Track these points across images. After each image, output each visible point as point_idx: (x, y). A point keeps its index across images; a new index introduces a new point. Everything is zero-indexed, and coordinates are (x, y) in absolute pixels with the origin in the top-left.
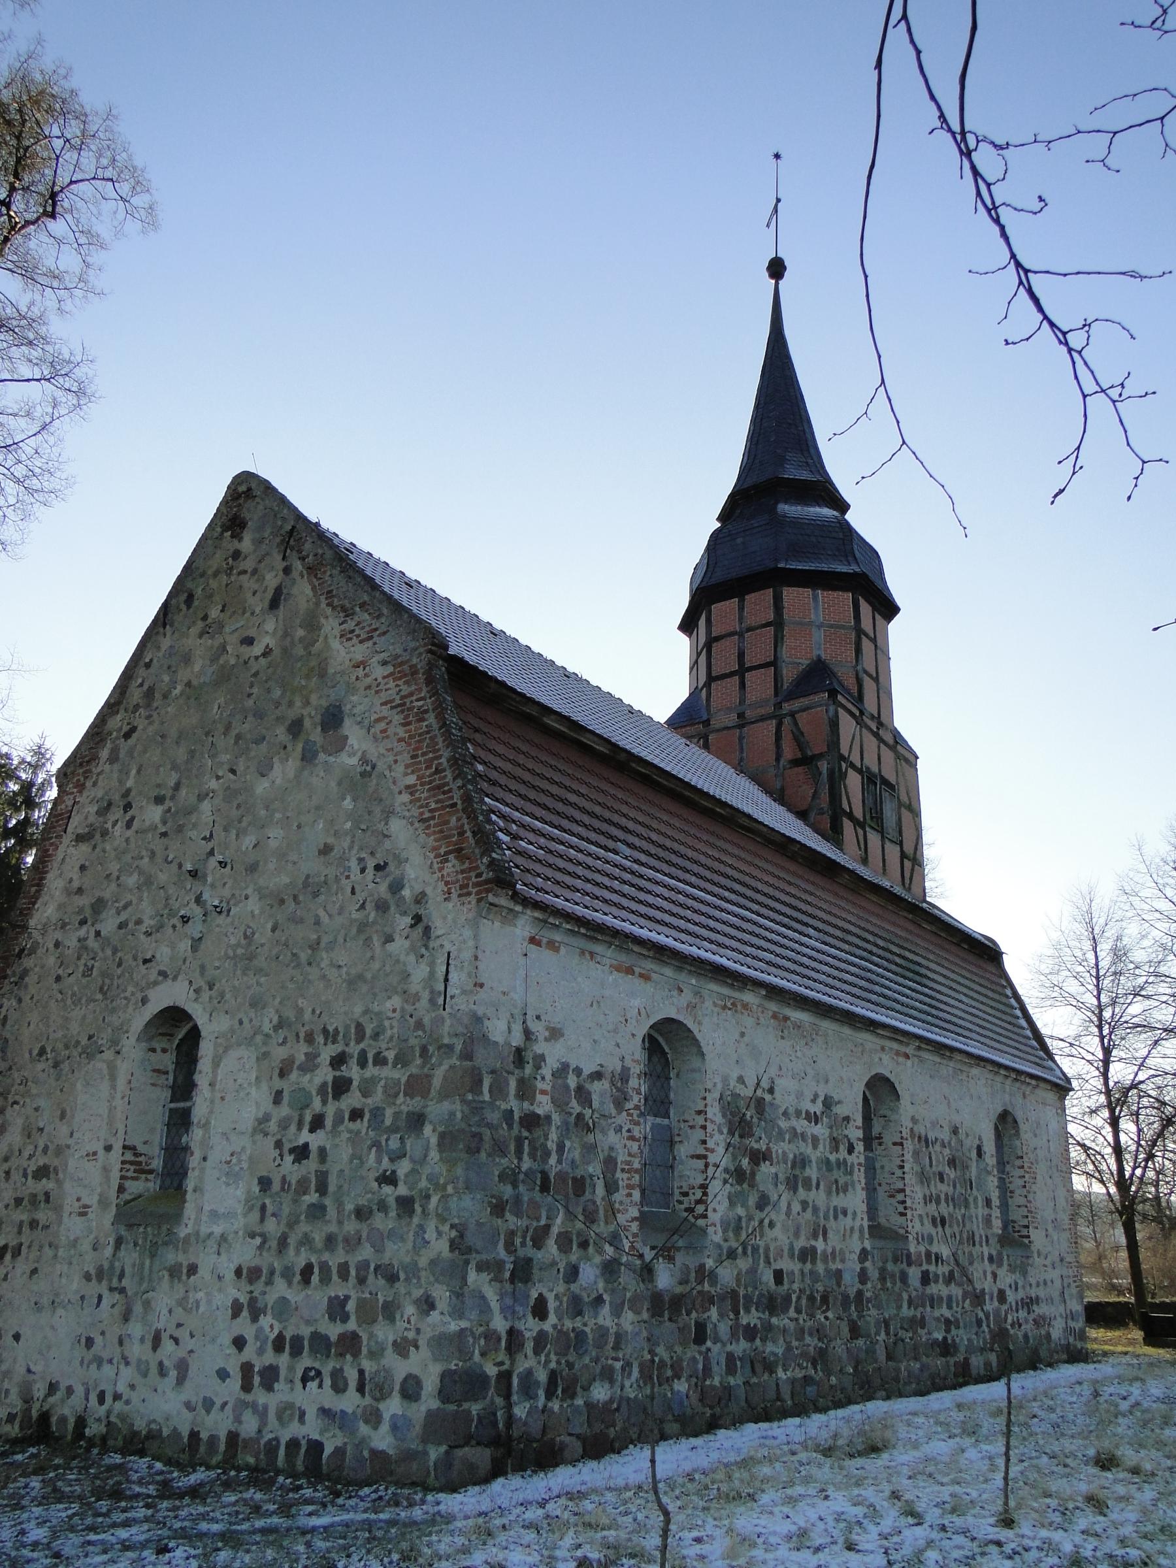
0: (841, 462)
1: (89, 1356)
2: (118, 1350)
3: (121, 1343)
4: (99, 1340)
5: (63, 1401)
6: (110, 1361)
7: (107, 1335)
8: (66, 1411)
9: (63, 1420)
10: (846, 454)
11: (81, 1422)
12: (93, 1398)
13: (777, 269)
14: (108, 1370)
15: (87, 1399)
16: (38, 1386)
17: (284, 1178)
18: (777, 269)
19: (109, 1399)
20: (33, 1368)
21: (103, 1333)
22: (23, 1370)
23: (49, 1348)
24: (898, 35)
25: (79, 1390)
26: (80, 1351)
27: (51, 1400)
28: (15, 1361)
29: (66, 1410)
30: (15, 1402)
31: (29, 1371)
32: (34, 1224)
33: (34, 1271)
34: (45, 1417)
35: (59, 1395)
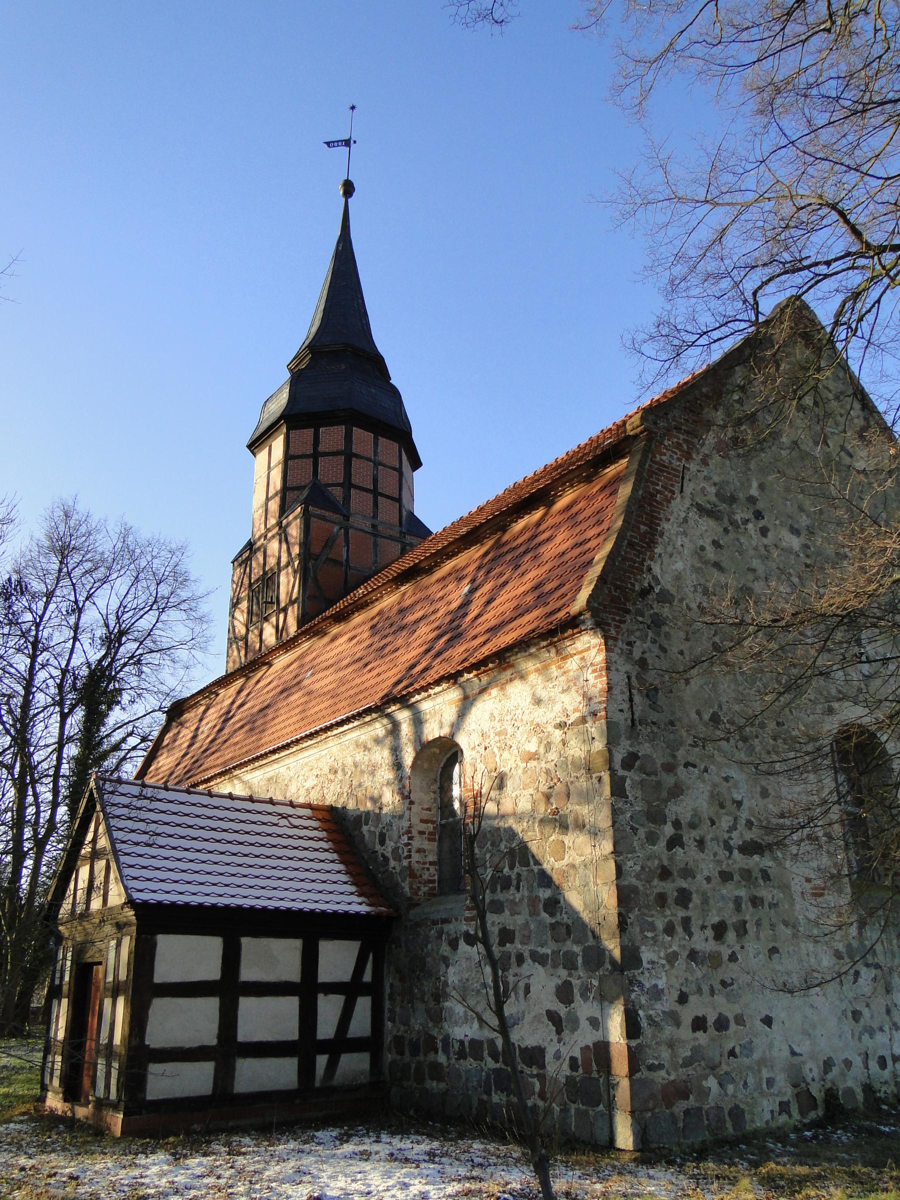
0: (385, 337)
1: (859, 1028)
2: (887, 1018)
3: (888, 1012)
4: (866, 1012)
5: (843, 1075)
6: (881, 1029)
7: (872, 1006)
8: (850, 1083)
9: (850, 1092)
10: (391, 334)
11: (868, 1089)
12: (873, 1065)
13: (349, 189)
14: (881, 1038)
15: (867, 1068)
16: (808, 1066)
17: (422, 821)
18: (349, 189)
19: (889, 1062)
20: (797, 1050)
21: (868, 1005)
22: (786, 1053)
23: (814, 1026)
24: (696, 343)
25: (858, 1061)
26: (848, 1025)
27: (830, 1076)
28: (771, 1046)
29: (851, 1082)
30: (784, 1089)
31: (793, 1053)
32: (756, 902)
33: (774, 951)
34: (831, 1095)
35: (835, 1071)
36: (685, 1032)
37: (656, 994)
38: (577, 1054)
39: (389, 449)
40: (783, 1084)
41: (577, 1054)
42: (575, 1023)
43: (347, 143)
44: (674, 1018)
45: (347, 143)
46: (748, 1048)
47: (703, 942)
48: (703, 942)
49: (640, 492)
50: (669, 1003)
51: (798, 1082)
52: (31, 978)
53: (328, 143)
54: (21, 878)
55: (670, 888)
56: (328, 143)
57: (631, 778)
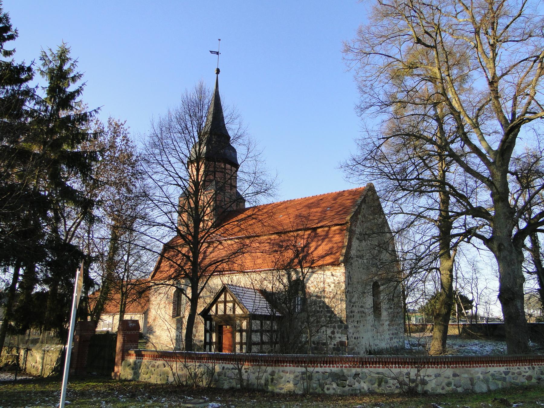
13: (218, 71)
18: (218, 71)
36: (353, 339)
37: (350, 333)
38: (336, 343)
39: (234, 169)
40: (364, 349)
41: (336, 343)
42: (335, 337)
43: (217, 53)
44: (352, 337)
45: (217, 53)
46: (360, 342)
47: (356, 324)
48: (356, 324)
49: (57, 100)
50: (351, 335)
51: (366, 349)
52: (541, 401)
53: (211, 52)
54: (11, 84)
55: (352, 315)
56: (211, 52)
57: (348, 294)
